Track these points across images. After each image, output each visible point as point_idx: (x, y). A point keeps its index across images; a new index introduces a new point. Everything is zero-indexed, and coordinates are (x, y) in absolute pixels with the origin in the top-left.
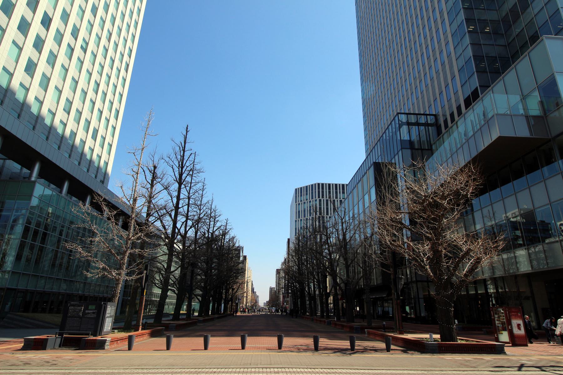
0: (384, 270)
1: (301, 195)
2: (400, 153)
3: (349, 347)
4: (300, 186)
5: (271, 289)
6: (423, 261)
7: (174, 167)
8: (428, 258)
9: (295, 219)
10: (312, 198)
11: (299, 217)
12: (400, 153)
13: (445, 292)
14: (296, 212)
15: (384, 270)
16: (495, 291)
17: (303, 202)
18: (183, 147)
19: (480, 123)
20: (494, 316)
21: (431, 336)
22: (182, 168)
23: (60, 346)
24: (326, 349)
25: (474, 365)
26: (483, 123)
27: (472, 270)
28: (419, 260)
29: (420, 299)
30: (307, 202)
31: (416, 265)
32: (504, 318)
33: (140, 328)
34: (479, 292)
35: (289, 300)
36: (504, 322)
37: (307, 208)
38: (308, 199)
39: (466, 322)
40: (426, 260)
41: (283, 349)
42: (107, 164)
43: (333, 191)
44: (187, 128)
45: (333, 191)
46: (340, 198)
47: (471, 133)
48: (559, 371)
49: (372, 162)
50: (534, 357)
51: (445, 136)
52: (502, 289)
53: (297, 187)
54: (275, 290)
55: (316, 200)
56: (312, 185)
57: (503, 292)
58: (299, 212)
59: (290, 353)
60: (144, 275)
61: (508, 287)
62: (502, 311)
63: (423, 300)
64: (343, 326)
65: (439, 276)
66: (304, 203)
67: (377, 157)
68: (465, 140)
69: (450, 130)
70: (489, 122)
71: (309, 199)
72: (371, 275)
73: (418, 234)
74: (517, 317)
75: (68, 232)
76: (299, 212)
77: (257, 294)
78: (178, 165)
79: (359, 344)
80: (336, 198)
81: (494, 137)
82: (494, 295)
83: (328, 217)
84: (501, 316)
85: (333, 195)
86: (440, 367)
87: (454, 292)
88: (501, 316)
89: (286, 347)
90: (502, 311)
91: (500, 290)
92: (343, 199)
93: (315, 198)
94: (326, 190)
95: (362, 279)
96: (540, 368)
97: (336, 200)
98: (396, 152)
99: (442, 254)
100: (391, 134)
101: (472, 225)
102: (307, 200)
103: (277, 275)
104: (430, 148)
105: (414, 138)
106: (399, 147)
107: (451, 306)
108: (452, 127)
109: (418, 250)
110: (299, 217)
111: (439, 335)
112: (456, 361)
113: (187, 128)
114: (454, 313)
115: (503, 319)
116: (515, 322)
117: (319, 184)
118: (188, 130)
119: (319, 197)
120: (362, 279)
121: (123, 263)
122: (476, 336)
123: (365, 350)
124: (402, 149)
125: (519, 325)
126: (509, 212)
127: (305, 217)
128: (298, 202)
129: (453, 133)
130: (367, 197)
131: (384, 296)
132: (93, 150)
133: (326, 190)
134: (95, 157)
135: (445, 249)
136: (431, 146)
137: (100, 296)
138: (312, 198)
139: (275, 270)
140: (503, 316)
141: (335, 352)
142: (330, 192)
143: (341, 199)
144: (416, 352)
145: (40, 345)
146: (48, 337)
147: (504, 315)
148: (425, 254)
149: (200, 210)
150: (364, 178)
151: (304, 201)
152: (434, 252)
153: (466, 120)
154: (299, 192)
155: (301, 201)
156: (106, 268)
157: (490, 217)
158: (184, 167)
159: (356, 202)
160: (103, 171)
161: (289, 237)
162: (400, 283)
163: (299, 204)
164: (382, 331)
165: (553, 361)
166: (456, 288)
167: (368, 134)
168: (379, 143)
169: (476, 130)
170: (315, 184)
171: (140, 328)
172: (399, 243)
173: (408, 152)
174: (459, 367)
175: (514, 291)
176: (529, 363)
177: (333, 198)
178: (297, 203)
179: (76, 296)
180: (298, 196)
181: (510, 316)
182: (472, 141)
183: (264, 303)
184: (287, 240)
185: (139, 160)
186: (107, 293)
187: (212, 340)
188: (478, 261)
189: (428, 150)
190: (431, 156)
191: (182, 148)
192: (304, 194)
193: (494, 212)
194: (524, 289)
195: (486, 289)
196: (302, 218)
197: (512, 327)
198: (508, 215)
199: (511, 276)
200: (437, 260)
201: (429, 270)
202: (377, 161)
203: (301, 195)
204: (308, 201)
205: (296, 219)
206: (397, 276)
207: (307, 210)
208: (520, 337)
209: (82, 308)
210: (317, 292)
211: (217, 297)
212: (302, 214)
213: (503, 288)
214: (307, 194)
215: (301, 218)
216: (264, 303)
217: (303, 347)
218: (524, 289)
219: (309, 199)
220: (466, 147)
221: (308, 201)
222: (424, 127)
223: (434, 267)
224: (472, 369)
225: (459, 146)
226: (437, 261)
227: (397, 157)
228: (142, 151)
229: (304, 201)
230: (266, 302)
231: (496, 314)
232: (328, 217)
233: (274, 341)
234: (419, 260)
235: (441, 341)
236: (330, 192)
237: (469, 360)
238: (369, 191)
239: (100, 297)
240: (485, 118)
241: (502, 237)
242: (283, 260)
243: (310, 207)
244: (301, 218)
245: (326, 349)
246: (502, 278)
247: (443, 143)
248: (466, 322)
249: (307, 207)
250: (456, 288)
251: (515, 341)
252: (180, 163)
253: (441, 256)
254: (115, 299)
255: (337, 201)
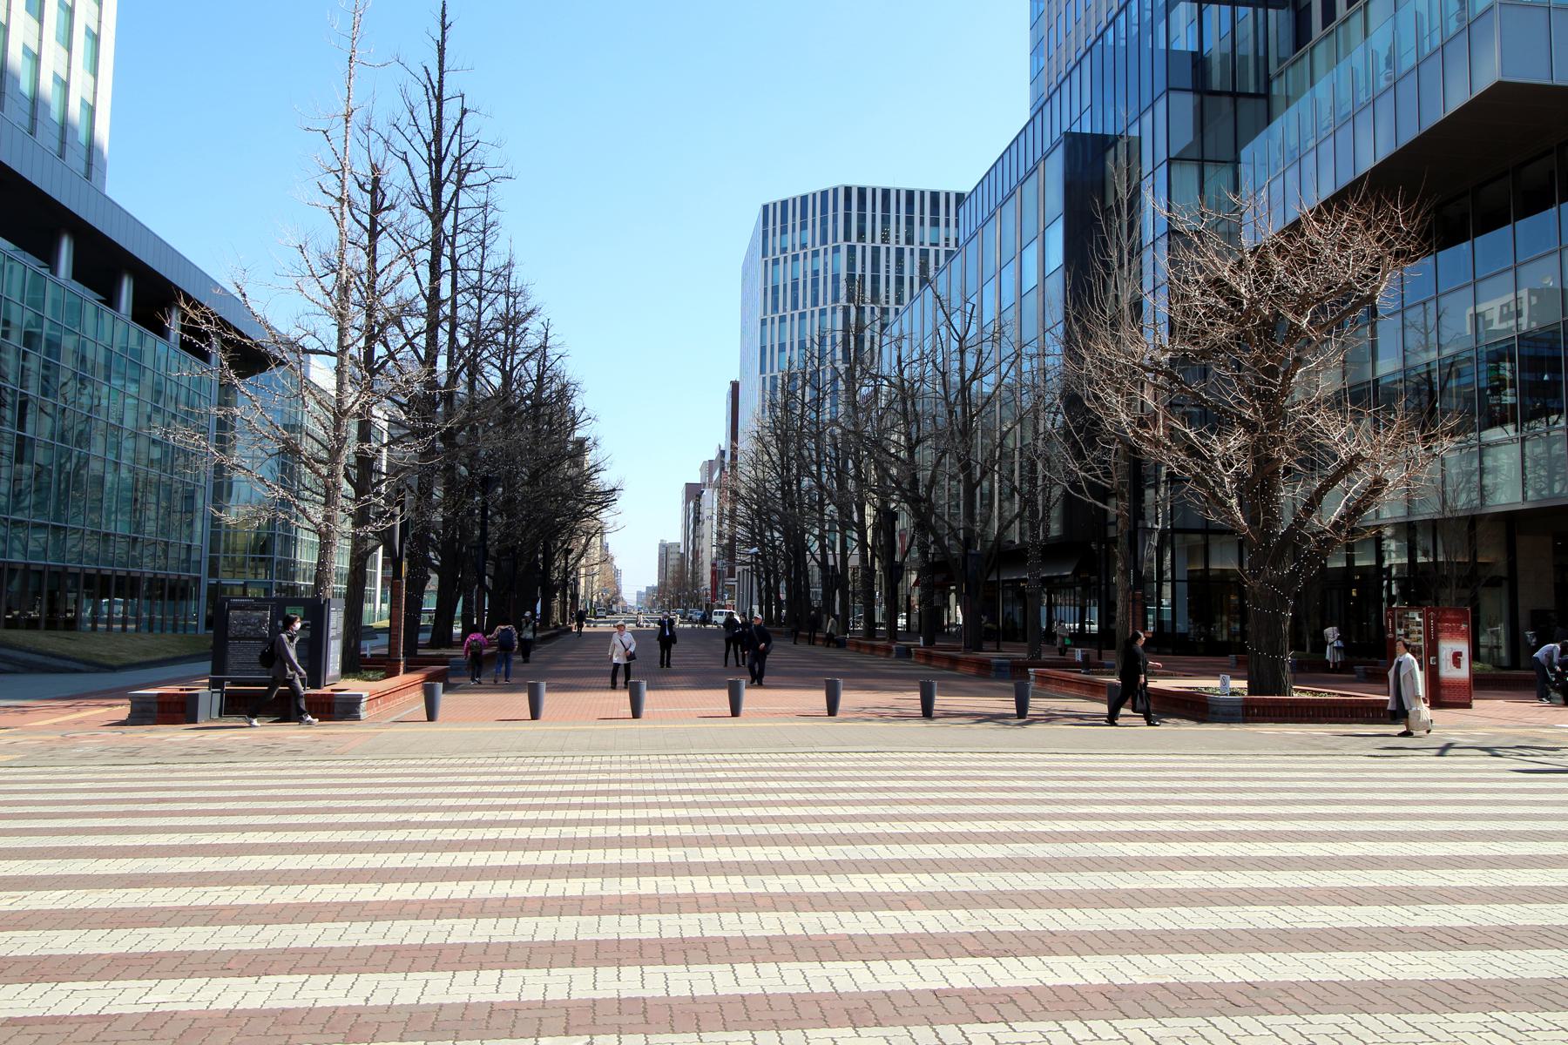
0: (1100, 505)
1: (784, 231)
2: (1161, 106)
3: (1015, 712)
4: (778, 197)
5: (665, 550)
6: (1221, 485)
7: (412, 156)
8: (1239, 476)
9: (759, 315)
10: (824, 241)
11: (775, 308)
12: (1161, 106)
13: (1275, 569)
14: (766, 290)
15: (1100, 505)
16: (1405, 560)
17: (790, 253)
18: (436, 85)
19: (1443, 26)
20: (1394, 631)
21: (1224, 684)
22: (439, 161)
23: (220, 715)
24: (948, 715)
25: (1332, 745)
26: (1453, 27)
27: (1355, 511)
28: (1212, 483)
29: (1177, 584)
30: (805, 254)
31: (1203, 495)
32: (1422, 636)
33: (401, 672)
34: (1357, 564)
35: (1421, 643)
36: (1420, 647)
37: (805, 276)
38: (809, 245)
39: (1308, 649)
40: (1231, 483)
41: (839, 716)
42: (91, 110)
43: (898, 213)
44: (444, 16)
45: (898, 213)
46: (922, 243)
47: (1408, 61)
48: (1533, 755)
49: (1056, 135)
50: (1484, 730)
51: (1321, 52)
52: (1425, 554)
53: (769, 200)
54: (682, 551)
55: (836, 250)
56: (824, 194)
57: (1429, 563)
58: (775, 289)
59: (868, 724)
60: (398, 522)
61: (1445, 552)
62: (1418, 619)
63: (1185, 585)
64: (954, 662)
65: (1262, 529)
66: (795, 258)
67: (1076, 114)
68: (1388, 79)
69: (1341, 30)
70: (1474, 28)
71: (813, 245)
72: (1049, 517)
73: (1218, 410)
74: (1454, 633)
75: (23, 366)
76: (775, 289)
77: (615, 563)
78: (426, 156)
79: (1037, 705)
80: (909, 240)
81: (1484, 82)
82: (1398, 573)
83: (877, 311)
84: (1413, 632)
85: (898, 231)
86: (1252, 749)
87: (1300, 571)
88: (1413, 632)
89: (844, 712)
90: (1418, 619)
91: (1421, 559)
92: (932, 244)
93: (835, 239)
94: (874, 212)
95: (1017, 522)
96: (1491, 751)
97: (907, 249)
98: (1146, 101)
99: (1278, 468)
100: (1135, 29)
101: (1369, 362)
102: (804, 246)
103: (687, 502)
104: (1262, 91)
105: (1215, 46)
106: (1161, 86)
107: (1285, 607)
108: (1346, 20)
109: (1210, 451)
110: (775, 308)
111: (1106, 706)
112: (1289, 738)
113: (444, 16)
114: (1290, 625)
115: (1419, 640)
116: (1447, 647)
117: (848, 190)
118: (447, 23)
119: (847, 237)
120: (1017, 522)
121: (334, 485)
122: (1338, 686)
123: (1050, 717)
124: (1168, 90)
125: (1456, 658)
126: (1487, 300)
127: (795, 307)
128: (774, 254)
129: (1348, 52)
130: (1031, 255)
131: (1066, 573)
132: (37, 59)
133: (874, 212)
134: (47, 86)
135: (1291, 455)
136: (1268, 83)
137: (119, 574)
138: (824, 241)
139: (682, 487)
140: (1420, 632)
141: (979, 722)
142: (886, 220)
143: (927, 246)
144: (1185, 721)
145: (178, 711)
146: (181, 690)
147: (1421, 628)
148: (1228, 464)
149: (480, 299)
150: (1026, 186)
151: (793, 250)
152: (1257, 461)
153: (1400, 12)
154: (777, 217)
155: (784, 250)
156: (289, 501)
157: (1426, 327)
158: (444, 159)
159: (990, 270)
160: (82, 137)
161: (736, 377)
162: (1147, 543)
163: (776, 262)
164: (1080, 672)
165: (1525, 738)
166: (1305, 559)
167: (1045, 13)
168: (1086, 62)
169: (1427, 51)
170: (835, 190)
171: (401, 672)
172: (1158, 432)
173: (1185, 103)
174: (1298, 748)
175: (1459, 563)
176: (1465, 740)
177: (897, 242)
178: (770, 258)
179: (76, 575)
180: (774, 230)
181: (1437, 631)
182: (1408, 88)
183: (639, 594)
184: (728, 387)
185: (341, 154)
186: (134, 562)
187: (549, 700)
188: (1378, 485)
189: (1256, 96)
190: (1263, 130)
191: (433, 87)
192: (794, 226)
193: (1441, 309)
194: (1491, 555)
195: (1380, 558)
196: (785, 310)
197: (1437, 660)
198: (1481, 308)
199: (1459, 518)
200: (1262, 482)
201: (1236, 509)
202: (1076, 129)
203: (784, 231)
204: (809, 250)
205: (765, 314)
206: (1140, 523)
207: (805, 282)
208: (1455, 686)
209: (266, 615)
210: (854, 561)
211: (1331, 632)
212: (786, 299)
213: (1431, 554)
214: (804, 226)
215: (781, 313)
216: (639, 594)
217: (893, 711)
218: (1491, 555)
219: (813, 245)
220: (1385, 106)
221: (809, 250)
222: (1250, 9)
223: (1253, 501)
224: (1328, 752)
225: (1362, 98)
226: (1263, 485)
227: (1147, 119)
228: (347, 121)
229: (793, 250)
230: (644, 590)
231: (1400, 626)
232: (877, 311)
233: (818, 698)
234: (1212, 483)
235: (1249, 694)
236: (886, 220)
237: (1320, 736)
238: (1041, 236)
239: (117, 577)
240: (1462, 9)
241: (1452, 424)
242: (713, 455)
243: (816, 273)
244: (781, 313)
245: (948, 715)
246: (1433, 526)
247: (1312, 84)
248: (1308, 649)
249: (805, 273)
250: (1305, 559)
251: (1440, 695)
252: (433, 148)
253: (1276, 472)
254: (325, 588)
255: (912, 251)
